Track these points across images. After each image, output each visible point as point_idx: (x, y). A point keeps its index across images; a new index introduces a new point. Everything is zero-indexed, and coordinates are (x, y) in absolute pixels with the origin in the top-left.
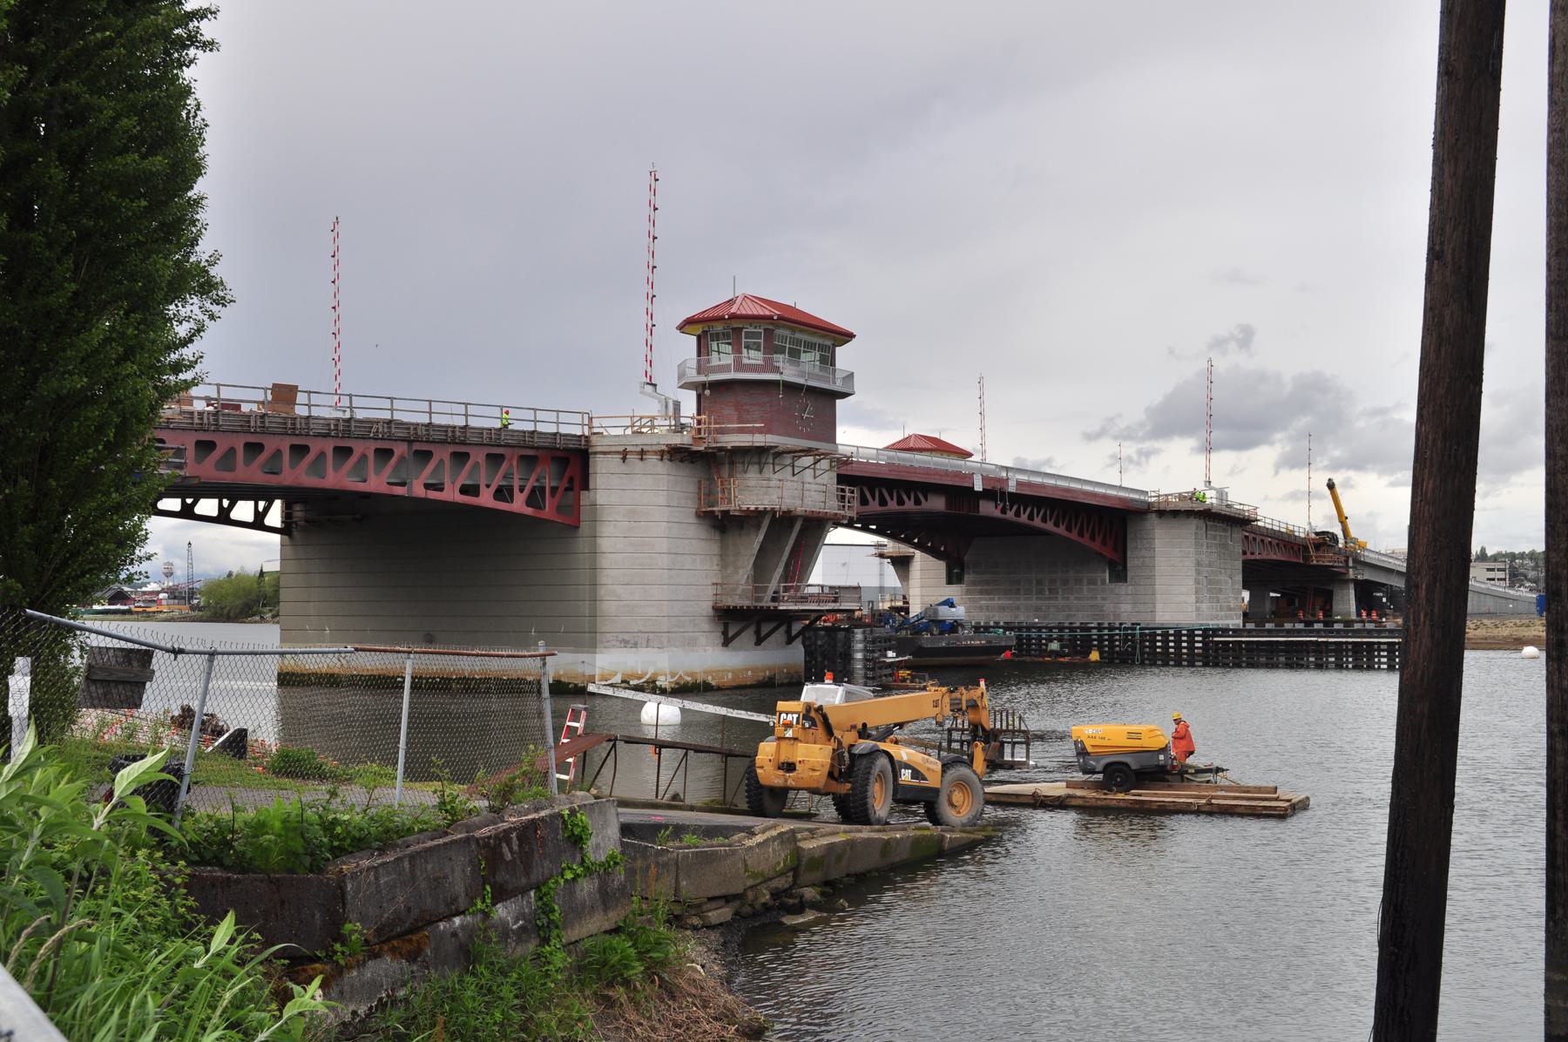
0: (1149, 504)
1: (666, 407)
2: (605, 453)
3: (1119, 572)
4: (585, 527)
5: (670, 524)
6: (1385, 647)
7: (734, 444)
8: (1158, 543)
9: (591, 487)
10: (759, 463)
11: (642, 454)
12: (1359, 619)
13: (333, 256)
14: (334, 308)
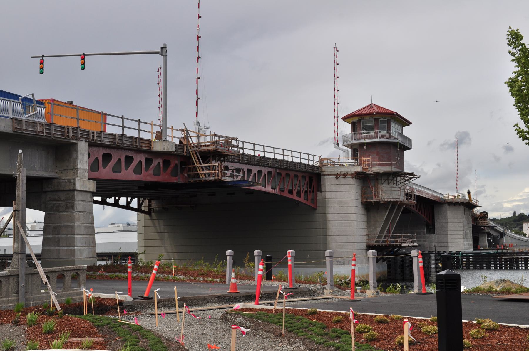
0: (445, 200)
2: (329, 175)
3: (431, 229)
4: (319, 209)
5: (356, 207)
7: (383, 171)
8: (448, 217)
9: (323, 190)
11: (345, 176)
13: (158, 84)
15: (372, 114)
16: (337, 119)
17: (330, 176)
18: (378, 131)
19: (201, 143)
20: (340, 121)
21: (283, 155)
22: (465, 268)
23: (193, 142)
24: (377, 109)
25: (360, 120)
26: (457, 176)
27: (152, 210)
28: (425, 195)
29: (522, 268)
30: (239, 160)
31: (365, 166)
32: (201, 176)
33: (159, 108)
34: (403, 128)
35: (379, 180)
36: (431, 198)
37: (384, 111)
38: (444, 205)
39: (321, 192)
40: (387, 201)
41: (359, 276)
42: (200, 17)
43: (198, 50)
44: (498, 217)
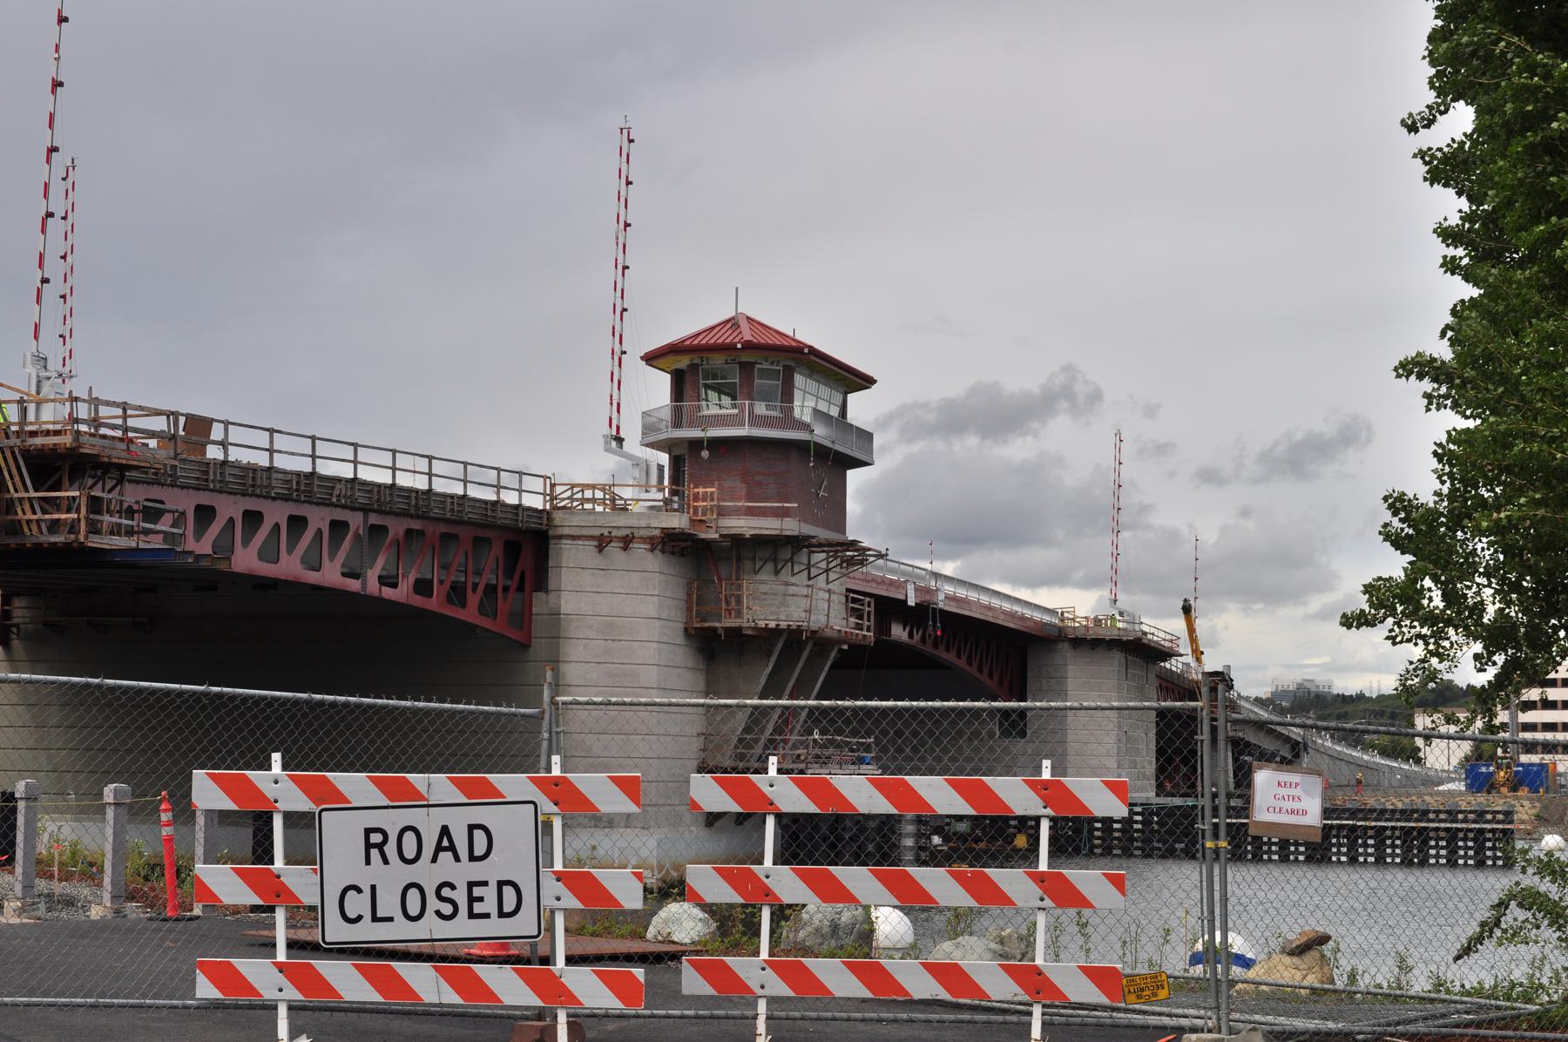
1: (647, 473)
2: (573, 538)
4: (539, 646)
5: (662, 646)
6: (1370, 833)
9: (552, 585)
10: (775, 561)
11: (627, 542)
12: (1239, 792)
14: (64, 297)
15: (730, 348)
16: (620, 359)
17: (580, 542)
18: (747, 402)
19: (102, 418)
20: (634, 363)
21: (394, 469)
22: (1119, 852)
23: (131, 416)
24: (749, 332)
25: (697, 365)
26: (1115, 554)
27: (15, 630)
28: (982, 610)
29: (1466, 862)
30: (206, 480)
31: (700, 513)
32: (26, 530)
33: (61, 297)
34: (850, 396)
35: (746, 562)
36: (1011, 625)
37: (778, 341)
38: (1060, 646)
39: (547, 591)
40: (766, 629)
41: (661, 868)
42: (66, 20)
43: (51, 126)
44: (1371, 692)
